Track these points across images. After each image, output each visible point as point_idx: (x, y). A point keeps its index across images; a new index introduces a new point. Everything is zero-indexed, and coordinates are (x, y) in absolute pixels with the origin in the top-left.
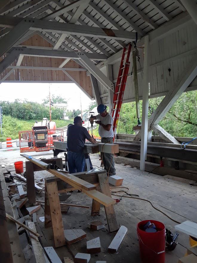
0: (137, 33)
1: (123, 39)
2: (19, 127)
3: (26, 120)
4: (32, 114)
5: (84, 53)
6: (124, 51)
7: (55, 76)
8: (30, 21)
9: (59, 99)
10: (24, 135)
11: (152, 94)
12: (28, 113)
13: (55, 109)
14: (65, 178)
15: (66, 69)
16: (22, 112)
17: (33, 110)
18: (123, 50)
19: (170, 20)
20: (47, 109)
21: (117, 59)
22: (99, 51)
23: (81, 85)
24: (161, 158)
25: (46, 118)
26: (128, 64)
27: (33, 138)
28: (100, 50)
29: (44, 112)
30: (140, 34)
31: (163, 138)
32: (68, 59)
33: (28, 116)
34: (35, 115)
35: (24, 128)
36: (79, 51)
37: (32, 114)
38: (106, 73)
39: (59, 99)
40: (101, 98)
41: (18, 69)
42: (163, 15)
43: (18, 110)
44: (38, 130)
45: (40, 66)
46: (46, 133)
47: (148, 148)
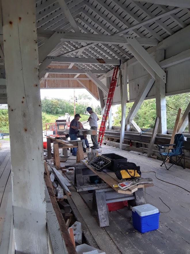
0: (120, 60)
1: (110, 65)
2: (47, 121)
3: (54, 114)
4: (58, 109)
5: (88, 71)
6: (115, 70)
7: (71, 83)
8: (51, 58)
9: (84, 95)
10: (51, 127)
11: (130, 100)
12: (55, 108)
13: (79, 105)
14: (61, 141)
15: (79, 79)
16: (51, 107)
17: (60, 106)
18: (114, 69)
19: (131, 58)
20: (71, 104)
21: (111, 74)
22: (116, 57)
23: (90, 90)
24: (131, 141)
25: (67, 114)
26: (116, 79)
27: (56, 129)
28: (118, 56)
29: (70, 107)
30: (122, 61)
31: (134, 129)
32: (78, 74)
33: (55, 111)
34: (61, 110)
35: (52, 121)
36: (87, 67)
37: (58, 109)
38: (106, 84)
39: (84, 95)
40: (103, 100)
41: (46, 80)
42: (178, 23)
43: (47, 105)
44: (60, 123)
45: (61, 77)
46: (65, 125)
47: (125, 135)
